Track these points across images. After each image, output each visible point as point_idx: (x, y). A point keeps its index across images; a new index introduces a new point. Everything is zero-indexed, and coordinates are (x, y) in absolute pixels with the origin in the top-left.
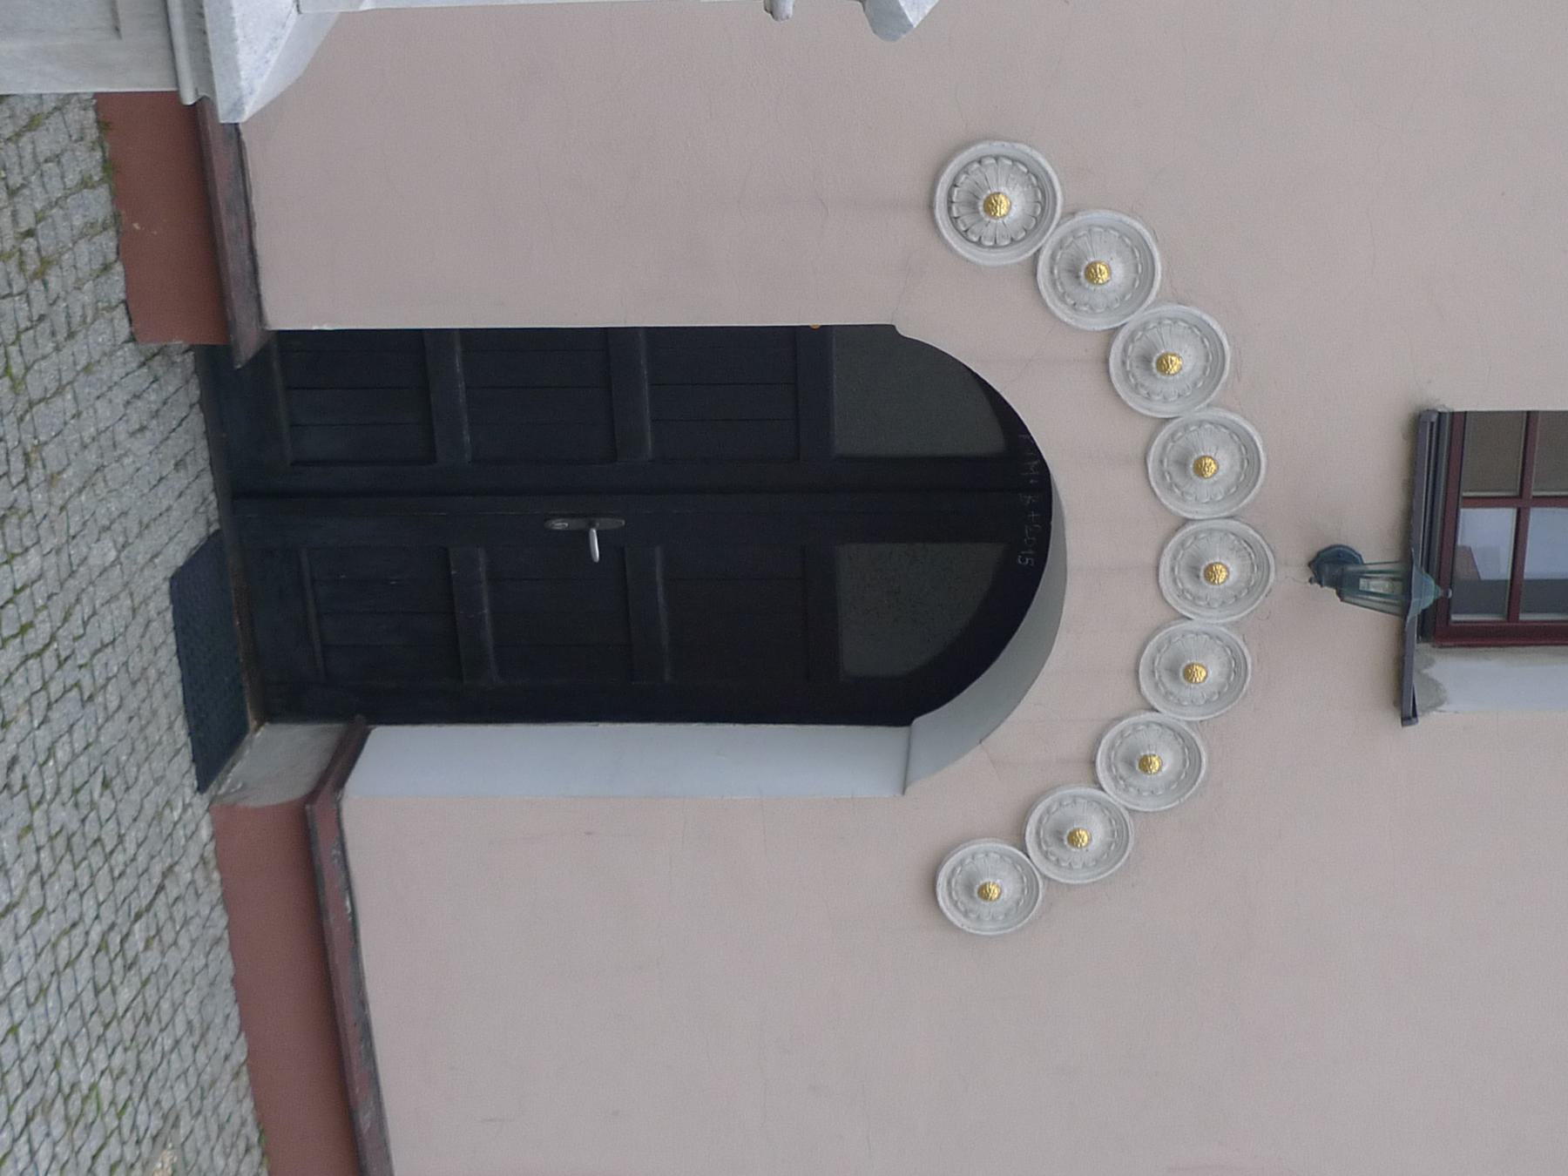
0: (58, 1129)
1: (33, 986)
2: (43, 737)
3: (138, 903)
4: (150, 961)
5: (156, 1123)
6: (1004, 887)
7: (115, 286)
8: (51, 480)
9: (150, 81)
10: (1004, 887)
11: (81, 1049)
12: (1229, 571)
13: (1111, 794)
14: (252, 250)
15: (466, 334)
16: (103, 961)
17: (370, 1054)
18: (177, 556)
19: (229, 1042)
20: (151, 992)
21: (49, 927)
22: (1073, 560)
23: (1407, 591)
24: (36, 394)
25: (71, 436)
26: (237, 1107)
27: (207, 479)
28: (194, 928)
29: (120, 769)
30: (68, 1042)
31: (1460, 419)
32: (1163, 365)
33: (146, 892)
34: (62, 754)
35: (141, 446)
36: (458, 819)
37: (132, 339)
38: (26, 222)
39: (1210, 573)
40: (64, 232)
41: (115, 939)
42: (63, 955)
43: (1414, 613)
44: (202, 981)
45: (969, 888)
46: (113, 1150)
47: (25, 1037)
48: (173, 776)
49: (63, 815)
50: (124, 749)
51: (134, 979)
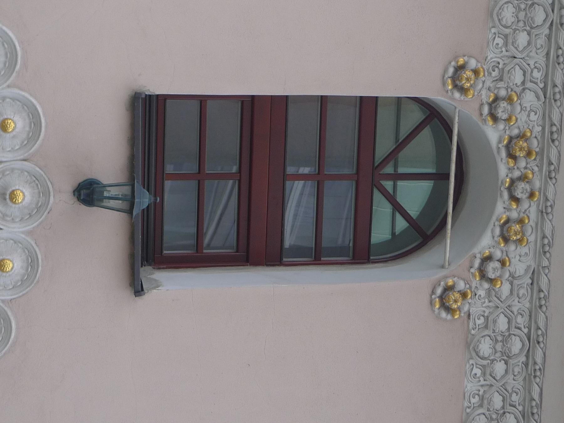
12: (25, 195)
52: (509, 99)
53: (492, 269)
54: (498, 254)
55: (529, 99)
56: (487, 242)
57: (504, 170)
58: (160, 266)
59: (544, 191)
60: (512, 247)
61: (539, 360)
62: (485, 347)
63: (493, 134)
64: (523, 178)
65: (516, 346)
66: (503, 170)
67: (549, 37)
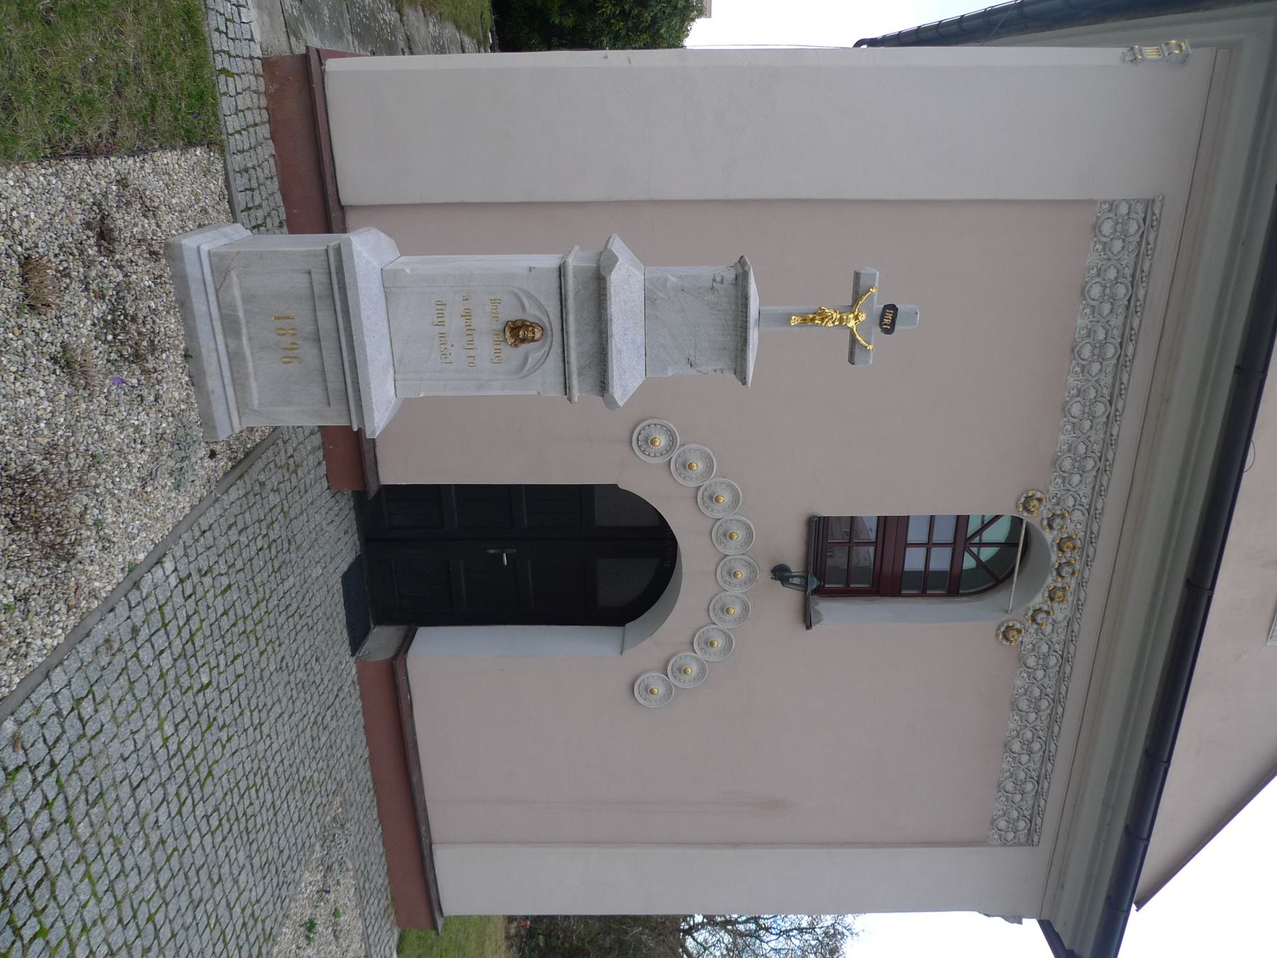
0: (298, 795)
1: (289, 743)
2: (294, 647)
3: (329, 703)
4: (333, 725)
5: (334, 787)
6: (659, 690)
7: (323, 470)
8: (298, 548)
9: (342, 422)
10: (659, 690)
11: (307, 764)
12: (743, 574)
13: (699, 655)
14: (375, 456)
15: (459, 487)
16: (315, 728)
17: (417, 753)
18: (345, 567)
19: (363, 751)
20: (333, 737)
21: (295, 719)
22: (685, 569)
23: (807, 583)
24: (293, 516)
25: (306, 530)
26: (365, 775)
27: (356, 536)
28: (349, 710)
29: (322, 652)
30: (302, 762)
31: (826, 519)
32: (717, 500)
33: (332, 698)
34: (301, 652)
35: (332, 528)
36: (449, 663)
37: (329, 488)
38: (290, 452)
39: (735, 575)
40: (304, 453)
41: (320, 719)
42: (300, 728)
43: (809, 591)
44: (352, 729)
45: (646, 689)
46: (318, 800)
47: (286, 763)
48: (342, 652)
49: (301, 675)
50: (324, 645)
51: (327, 733)
52: (1063, 516)
53: (1040, 617)
54: (1046, 608)
55: (1077, 515)
56: (1039, 600)
57: (1054, 557)
58: (1006, 15)
59: (1082, 572)
60: (1055, 605)
61: (1068, 672)
62: (1031, 662)
63: (1049, 536)
64: (1068, 563)
65: (1133, 228)
66: (1054, 558)
67: (1096, 477)
